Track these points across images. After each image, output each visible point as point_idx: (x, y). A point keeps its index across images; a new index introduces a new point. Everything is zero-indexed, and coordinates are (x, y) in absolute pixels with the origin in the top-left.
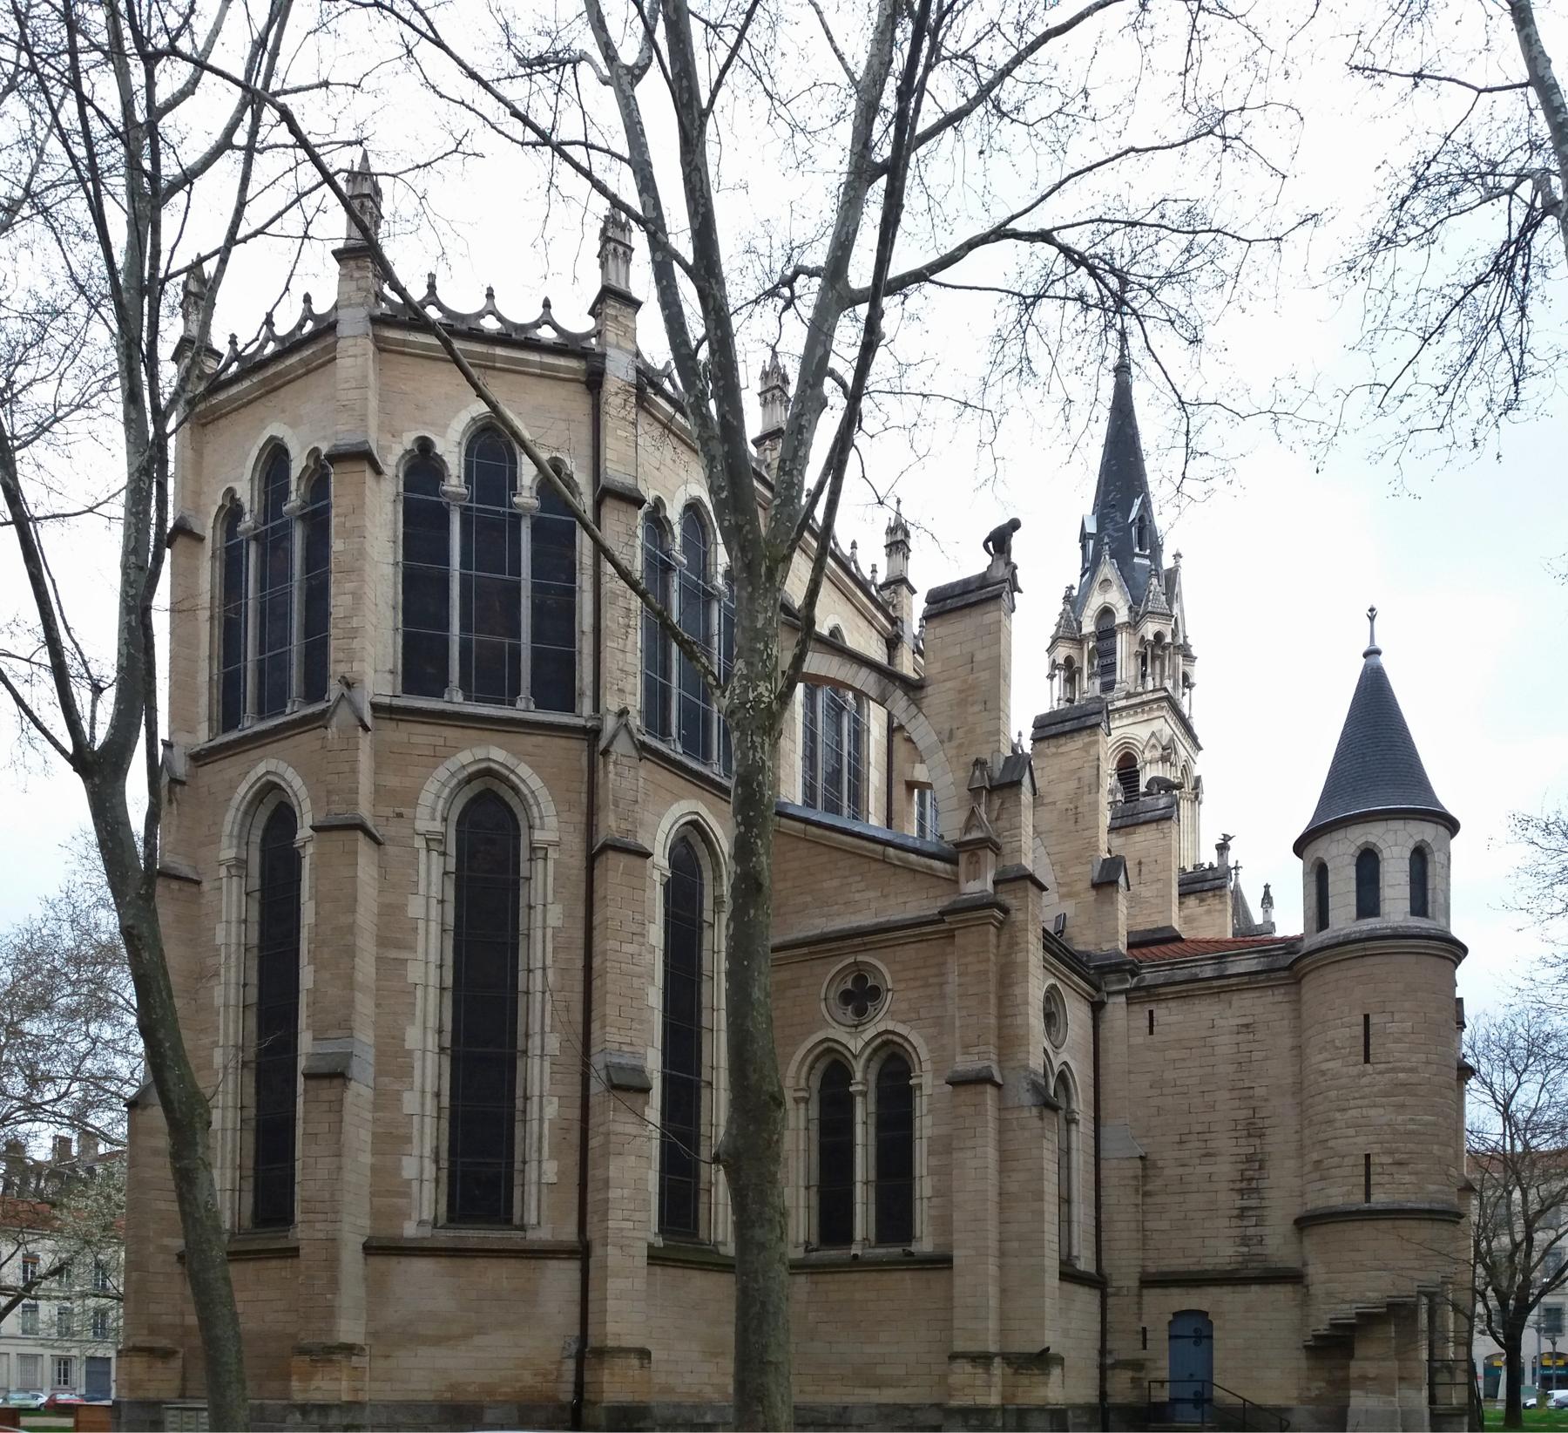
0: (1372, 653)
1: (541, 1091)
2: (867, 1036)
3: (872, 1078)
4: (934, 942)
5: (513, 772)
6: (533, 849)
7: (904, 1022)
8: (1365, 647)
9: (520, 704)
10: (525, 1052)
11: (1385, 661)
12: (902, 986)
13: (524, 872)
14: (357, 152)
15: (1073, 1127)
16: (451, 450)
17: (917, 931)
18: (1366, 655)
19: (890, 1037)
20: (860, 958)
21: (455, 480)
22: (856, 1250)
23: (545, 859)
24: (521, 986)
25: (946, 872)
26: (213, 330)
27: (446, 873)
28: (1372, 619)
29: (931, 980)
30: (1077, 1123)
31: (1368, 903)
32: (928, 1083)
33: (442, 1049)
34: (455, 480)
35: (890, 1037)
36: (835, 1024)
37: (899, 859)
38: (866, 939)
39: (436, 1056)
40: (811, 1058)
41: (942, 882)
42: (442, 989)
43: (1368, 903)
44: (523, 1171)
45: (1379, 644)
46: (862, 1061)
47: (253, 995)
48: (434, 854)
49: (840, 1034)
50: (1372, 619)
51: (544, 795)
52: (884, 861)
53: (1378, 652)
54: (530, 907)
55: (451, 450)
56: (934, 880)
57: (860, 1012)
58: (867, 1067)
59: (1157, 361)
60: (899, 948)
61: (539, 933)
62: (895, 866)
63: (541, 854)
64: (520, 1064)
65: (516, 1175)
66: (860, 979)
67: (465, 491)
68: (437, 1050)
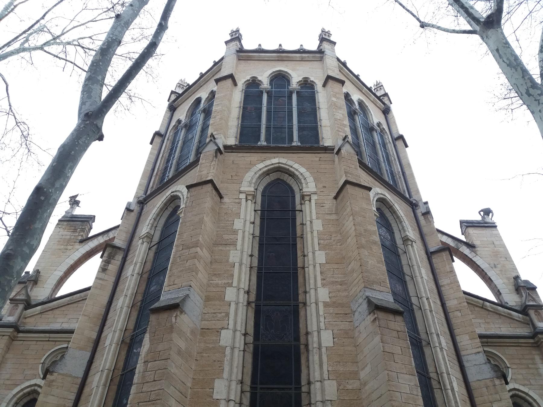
1: (318, 326)
4: (524, 348)
5: (292, 167)
6: (303, 197)
7: (524, 385)
10: (305, 304)
12: (515, 367)
13: (298, 207)
14: (327, 378)
17: (516, 340)
19: (517, 392)
23: (310, 201)
24: (300, 264)
25: (519, 317)
26: (310, 378)
29: (530, 366)
33: (249, 303)
35: (517, 392)
37: (492, 308)
38: (490, 340)
39: (245, 307)
41: (515, 322)
42: (251, 268)
44: (309, 393)
48: (249, 202)
51: (307, 174)
52: (482, 308)
54: (302, 224)
55: (265, 83)
56: (512, 320)
60: (506, 348)
61: (309, 235)
62: (490, 311)
63: (307, 198)
64: (302, 313)
65: (304, 396)
68: (245, 303)
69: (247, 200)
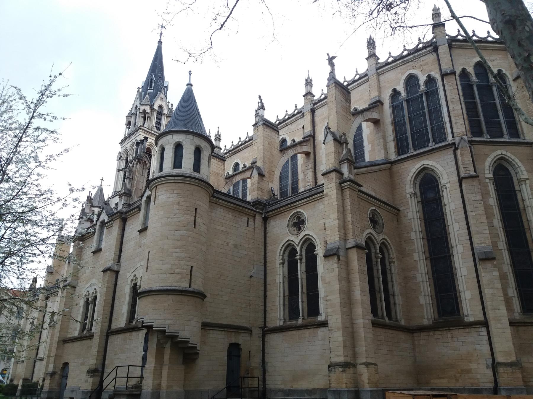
0: (190, 85)
2: (300, 237)
3: (304, 253)
8: (188, 82)
9: (430, 145)
11: (193, 88)
15: (392, 264)
16: (470, 70)
18: (187, 85)
20: (298, 210)
21: (403, 94)
22: (300, 321)
27: (418, 202)
28: (190, 74)
30: (394, 262)
31: (177, 163)
32: (320, 252)
34: (474, 79)
36: (290, 235)
40: (284, 248)
43: (177, 163)
45: (192, 82)
46: (299, 247)
47: (428, 255)
49: (292, 238)
50: (190, 74)
53: (192, 85)
57: (299, 229)
58: (301, 249)
59: (419, 26)
66: (299, 218)
67: (478, 80)
69: (411, 197)
